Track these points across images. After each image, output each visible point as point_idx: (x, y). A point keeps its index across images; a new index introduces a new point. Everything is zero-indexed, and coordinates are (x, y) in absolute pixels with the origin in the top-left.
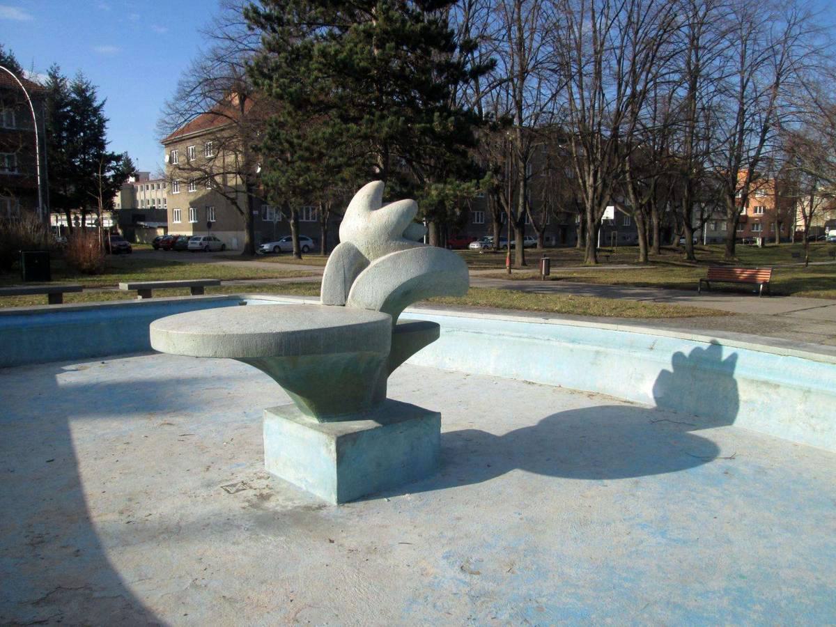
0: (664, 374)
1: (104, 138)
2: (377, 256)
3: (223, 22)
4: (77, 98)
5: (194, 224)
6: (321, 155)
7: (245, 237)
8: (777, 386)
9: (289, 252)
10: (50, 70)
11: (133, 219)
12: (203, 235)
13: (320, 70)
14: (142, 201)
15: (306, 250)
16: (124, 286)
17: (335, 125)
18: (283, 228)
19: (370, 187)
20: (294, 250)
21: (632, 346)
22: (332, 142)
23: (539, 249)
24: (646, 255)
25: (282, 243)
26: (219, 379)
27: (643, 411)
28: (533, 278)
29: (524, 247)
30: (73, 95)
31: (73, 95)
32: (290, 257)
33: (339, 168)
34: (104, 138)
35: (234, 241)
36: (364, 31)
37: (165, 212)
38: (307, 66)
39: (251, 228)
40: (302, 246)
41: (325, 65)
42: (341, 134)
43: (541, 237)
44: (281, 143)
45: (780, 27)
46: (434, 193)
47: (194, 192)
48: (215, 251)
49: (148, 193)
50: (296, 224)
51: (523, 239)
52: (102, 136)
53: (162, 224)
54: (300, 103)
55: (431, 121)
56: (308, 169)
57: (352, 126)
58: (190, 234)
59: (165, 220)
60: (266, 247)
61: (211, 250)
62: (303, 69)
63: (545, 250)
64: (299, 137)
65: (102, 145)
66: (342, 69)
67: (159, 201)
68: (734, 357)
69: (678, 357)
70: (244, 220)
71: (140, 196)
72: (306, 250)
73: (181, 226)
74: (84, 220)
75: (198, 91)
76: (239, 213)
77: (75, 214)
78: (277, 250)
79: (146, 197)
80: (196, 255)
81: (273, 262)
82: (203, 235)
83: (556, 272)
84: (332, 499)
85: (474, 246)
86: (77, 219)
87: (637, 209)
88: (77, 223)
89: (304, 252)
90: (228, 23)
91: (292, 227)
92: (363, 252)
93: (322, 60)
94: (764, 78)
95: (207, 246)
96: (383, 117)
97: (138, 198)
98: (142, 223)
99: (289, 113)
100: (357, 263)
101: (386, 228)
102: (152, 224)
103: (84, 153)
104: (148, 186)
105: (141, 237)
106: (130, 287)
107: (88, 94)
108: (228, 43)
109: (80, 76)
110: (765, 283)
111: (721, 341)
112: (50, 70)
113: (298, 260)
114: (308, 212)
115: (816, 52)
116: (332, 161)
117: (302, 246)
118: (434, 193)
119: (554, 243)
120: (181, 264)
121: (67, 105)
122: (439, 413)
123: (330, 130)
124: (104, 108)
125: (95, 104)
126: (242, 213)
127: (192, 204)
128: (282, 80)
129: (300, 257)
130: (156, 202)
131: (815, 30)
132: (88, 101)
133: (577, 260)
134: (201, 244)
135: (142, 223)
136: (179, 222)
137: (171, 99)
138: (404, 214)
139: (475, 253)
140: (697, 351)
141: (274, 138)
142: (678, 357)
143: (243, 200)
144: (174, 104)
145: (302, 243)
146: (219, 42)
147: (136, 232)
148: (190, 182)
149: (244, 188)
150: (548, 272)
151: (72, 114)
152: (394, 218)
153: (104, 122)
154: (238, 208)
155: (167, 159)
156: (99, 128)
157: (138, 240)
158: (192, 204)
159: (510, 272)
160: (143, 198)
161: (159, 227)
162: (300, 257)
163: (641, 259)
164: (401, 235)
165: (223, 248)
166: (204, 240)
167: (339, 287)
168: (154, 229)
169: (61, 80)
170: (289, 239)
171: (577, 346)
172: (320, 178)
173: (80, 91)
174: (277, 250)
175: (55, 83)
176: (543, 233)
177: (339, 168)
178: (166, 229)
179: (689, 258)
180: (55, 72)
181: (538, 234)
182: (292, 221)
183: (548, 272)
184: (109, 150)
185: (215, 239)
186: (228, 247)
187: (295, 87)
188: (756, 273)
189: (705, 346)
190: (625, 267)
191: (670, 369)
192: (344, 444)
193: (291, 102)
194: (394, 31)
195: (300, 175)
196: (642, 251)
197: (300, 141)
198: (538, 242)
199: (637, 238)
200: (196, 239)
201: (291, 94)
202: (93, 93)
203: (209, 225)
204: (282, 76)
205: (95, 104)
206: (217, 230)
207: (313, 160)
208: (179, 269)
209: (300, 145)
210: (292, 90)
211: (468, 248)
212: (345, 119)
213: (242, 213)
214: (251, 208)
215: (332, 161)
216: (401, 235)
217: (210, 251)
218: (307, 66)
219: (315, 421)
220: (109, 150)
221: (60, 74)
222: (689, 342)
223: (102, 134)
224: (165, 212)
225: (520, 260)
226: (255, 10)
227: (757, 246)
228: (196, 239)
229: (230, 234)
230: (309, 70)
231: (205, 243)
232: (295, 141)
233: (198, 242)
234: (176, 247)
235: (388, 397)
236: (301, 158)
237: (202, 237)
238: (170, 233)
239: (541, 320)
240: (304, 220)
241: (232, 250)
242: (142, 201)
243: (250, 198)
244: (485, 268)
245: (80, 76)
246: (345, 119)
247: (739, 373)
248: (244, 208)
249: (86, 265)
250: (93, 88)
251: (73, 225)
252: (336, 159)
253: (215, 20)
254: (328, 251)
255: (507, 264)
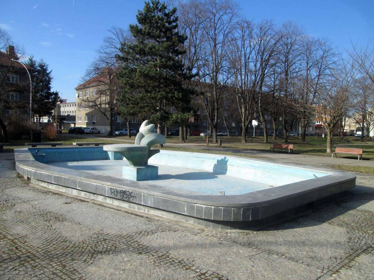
0: (215, 164)
1: (50, 85)
2: (146, 135)
3: (104, 47)
4: (40, 69)
5: (87, 122)
6: (138, 103)
7: (108, 128)
8: (234, 166)
9: (126, 135)
10: (30, 57)
11: (63, 120)
12: (91, 127)
13: (139, 76)
14: (63, 112)
15: (133, 134)
16: (74, 144)
17: (143, 94)
18: (124, 125)
19: (146, 121)
20: (128, 134)
21: (210, 159)
22: (142, 99)
23: (228, 137)
24: (267, 140)
25: (123, 131)
26: (109, 166)
27: (210, 173)
28: (216, 147)
29: (217, 136)
30: (39, 68)
31: (39, 68)
32: (127, 137)
33: (144, 107)
34: (50, 85)
35: (104, 130)
36: (154, 65)
37: (75, 117)
38: (135, 74)
39: (111, 125)
40: (131, 133)
41: (140, 75)
42: (145, 97)
43: (230, 132)
44: (125, 98)
45: (321, 53)
46: (174, 117)
47: (88, 110)
48: (96, 134)
49: (66, 108)
50: (130, 124)
51: (216, 132)
52: (49, 85)
53: (73, 122)
54: (132, 86)
55: (174, 94)
56: (134, 107)
57: (149, 94)
58: (85, 126)
59: (75, 120)
60: (117, 133)
61: (95, 133)
62: (134, 75)
63: (231, 137)
64: (132, 97)
65: (49, 89)
66: (146, 76)
67: (70, 112)
68: (228, 160)
69: (218, 161)
70: (108, 122)
71: (62, 109)
72: (133, 134)
73: (81, 123)
74: (40, 119)
75: (93, 73)
76: (107, 119)
77: (36, 117)
78: (121, 134)
79: (65, 110)
80: (88, 135)
81: (120, 139)
82: (91, 127)
83: (223, 145)
84: (136, 180)
85: (202, 134)
86: (37, 119)
87: (263, 122)
88: (37, 121)
89: (132, 135)
90: (106, 48)
91: (128, 126)
92: (143, 134)
93: (140, 74)
94: (314, 73)
95: (92, 132)
96: (159, 91)
97: (61, 110)
98: (65, 121)
99: (129, 89)
100: (142, 136)
101: (148, 129)
102: (69, 122)
103: (42, 92)
104: (68, 105)
105: (64, 127)
106: (77, 144)
107: (45, 68)
108: (105, 55)
109: (42, 60)
110: (291, 149)
111: (226, 157)
112: (30, 57)
113: (130, 138)
114: (134, 119)
115: (334, 63)
116: (142, 105)
117: (131, 133)
118: (174, 117)
119: (237, 134)
120: (85, 138)
121: (35, 72)
122: (157, 167)
123: (141, 95)
124: (51, 73)
125: (48, 72)
126: (108, 119)
127: (86, 114)
128: (127, 79)
129: (131, 137)
130: (69, 112)
131: (334, 55)
132: (45, 70)
133: (239, 141)
134: (90, 131)
135: (65, 121)
136: (81, 121)
137: (83, 76)
138: (152, 127)
139: (202, 137)
140: (222, 159)
141: (124, 97)
142: (218, 161)
143: (108, 114)
144: (84, 78)
145: (132, 132)
146: (102, 55)
147: (62, 125)
148: (90, 107)
149: (109, 110)
150: (221, 145)
151: (38, 75)
152: (150, 128)
153: (51, 79)
154: (107, 117)
155: (77, 95)
156: (49, 82)
157: (63, 128)
158: (86, 114)
159: (208, 144)
160: (63, 110)
161: (72, 123)
162: (131, 137)
163: (265, 142)
164: (152, 131)
165: (99, 133)
166: (91, 129)
167: (139, 140)
168: (70, 124)
169: (34, 62)
170: (126, 130)
171: (199, 159)
172: (138, 110)
173: (42, 66)
174: (121, 134)
175: (32, 63)
176: (230, 130)
177: (144, 107)
178: (75, 124)
179: (285, 142)
180: (32, 58)
181: (228, 131)
182: (128, 123)
183: (221, 145)
184: (52, 90)
185: (95, 129)
186: (101, 132)
187: (131, 81)
188: (288, 146)
189: (223, 158)
190: (257, 144)
191: (216, 163)
192: (138, 170)
193: (129, 86)
194: (163, 64)
195: (131, 109)
196: (265, 138)
197: (132, 98)
198: (228, 133)
199: (273, 133)
200: (88, 129)
201: (129, 83)
202: (47, 67)
203: (94, 123)
204: (127, 77)
205: (48, 72)
206: (97, 125)
207: (135, 104)
208: (87, 140)
209: (132, 100)
210: (130, 82)
211: (200, 135)
212: (147, 92)
213: (108, 119)
214: (112, 117)
215: (142, 105)
216: (152, 131)
217: (94, 134)
218: (135, 74)
219: (133, 166)
220: (52, 90)
221: (34, 59)
222: (220, 157)
223: (49, 84)
224: (75, 117)
225: (215, 140)
226: (119, 56)
227: (322, 138)
228: (88, 129)
229: (102, 127)
230: (136, 76)
231: (92, 131)
232: (130, 98)
233: (89, 130)
234: (79, 132)
235: (148, 164)
236: (132, 103)
237: (91, 128)
238: (76, 126)
239: (191, 153)
240: (133, 122)
241: (103, 133)
242: (63, 112)
243: (112, 114)
244: (201, 143)
245: (42, 60)
246: (147, 92)
247: (228, 163)
248: (109, 117)
249: (51, 137)
250: (47, 65)
251: (35, 121)
252: (144, 104)
253: (101, 46)
254: (135, 135)
255: (207, 141)
